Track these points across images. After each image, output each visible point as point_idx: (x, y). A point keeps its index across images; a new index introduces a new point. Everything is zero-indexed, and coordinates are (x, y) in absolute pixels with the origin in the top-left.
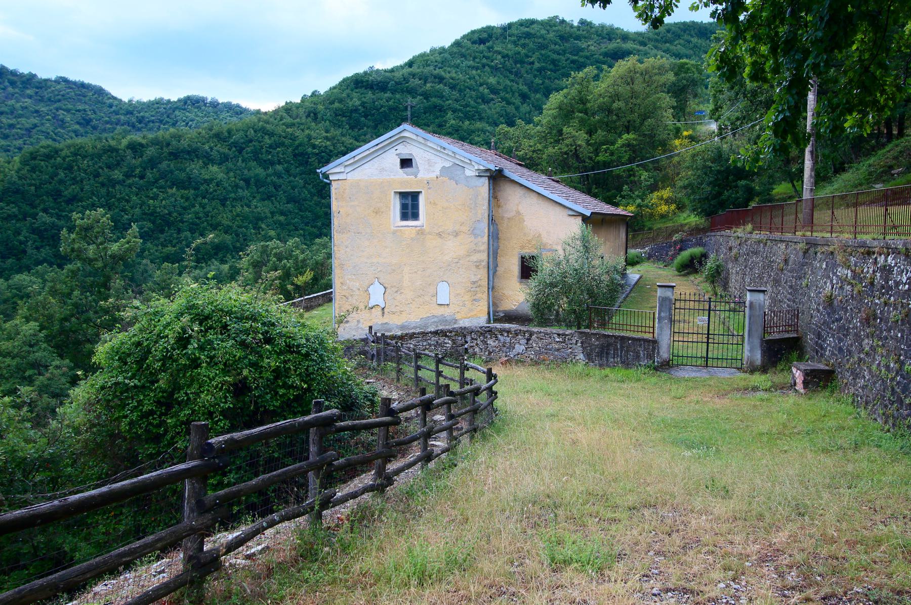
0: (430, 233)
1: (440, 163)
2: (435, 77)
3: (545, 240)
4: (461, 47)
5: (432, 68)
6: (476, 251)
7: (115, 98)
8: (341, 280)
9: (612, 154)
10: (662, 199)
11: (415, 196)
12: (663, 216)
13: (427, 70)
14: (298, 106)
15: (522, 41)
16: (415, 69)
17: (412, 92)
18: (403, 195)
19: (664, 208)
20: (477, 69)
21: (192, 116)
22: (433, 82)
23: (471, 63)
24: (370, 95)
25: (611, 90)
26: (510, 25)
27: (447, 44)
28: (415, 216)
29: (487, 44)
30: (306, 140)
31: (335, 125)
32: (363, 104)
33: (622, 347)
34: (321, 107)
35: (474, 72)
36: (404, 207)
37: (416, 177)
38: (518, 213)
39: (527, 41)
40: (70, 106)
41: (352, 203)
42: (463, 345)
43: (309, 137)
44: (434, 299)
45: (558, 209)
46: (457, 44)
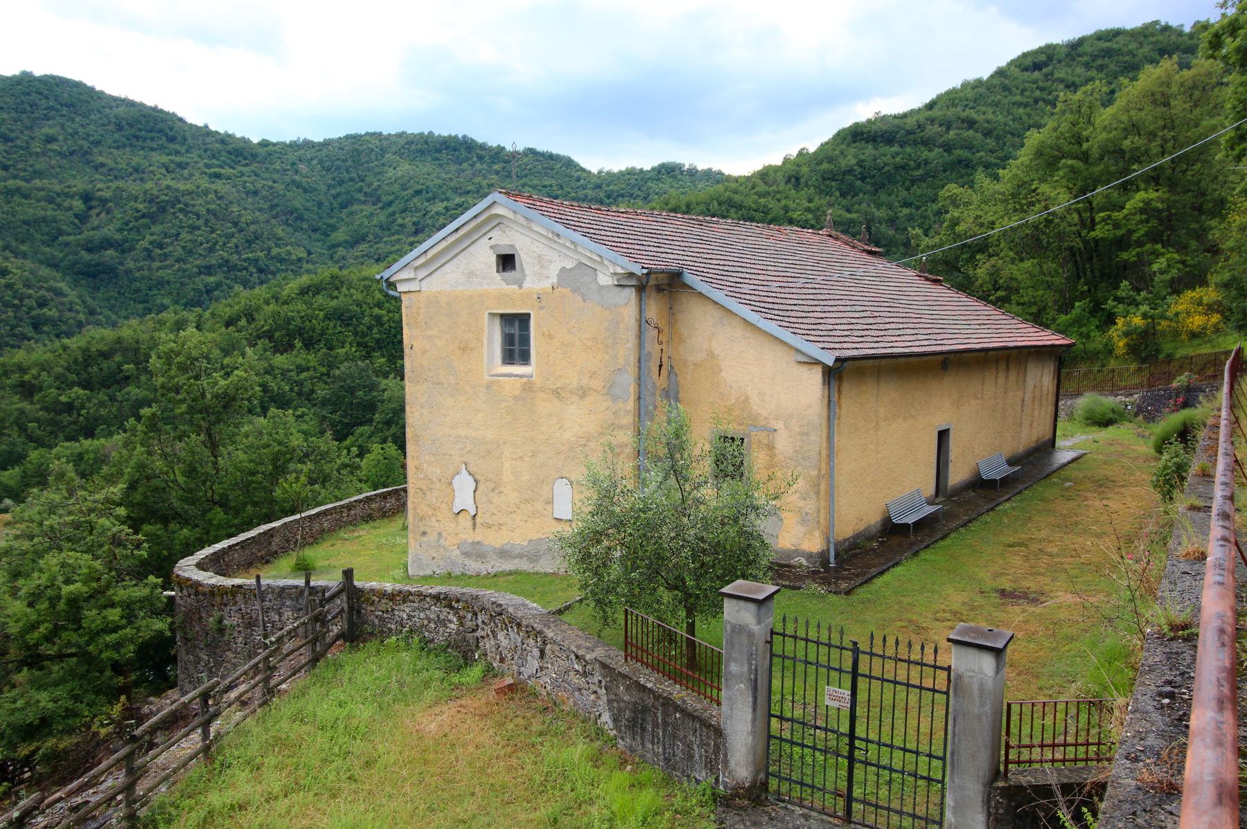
0: (542, 390)
1: (559, 262)
2: (963, 121)
3: (756, 409)
4: (1006, 77)
5: (959, 109)
6: (615, 427)
7: (583, 170)
8: (416, 463)
9: (1116, 226)
10: (1200, 304)
11: (524, 319)
12: (1194, 335)
13: (951, 113)
14: (776, 169)
15: (1099, 62)
16: (936, 113)
17: (927, 143)
18: (507, 319)
19: (1197, 321)
20: (1026, 105)
21: (666, 187)
22: (959, 129)
23: (1018, 98)
24: (869, 151)
25: (1124, 118)
26: (1082, 41)
27: (985, 73)
28: (525, 358)
29: (1045, 70)
30: (782, 212)
31: (821, 192)
32: (860, 163)
33: (665, 724)
34: (805, 169)
35: (1021, 110)
36: (508, 340)
37: (521, 287)
38: (711, 353)
39: (1107, 60)
40: (535, 182)
41: (430, 333)
42: (474, 631)
43: (786, 209)
44: (548, 507)
45: (779, 349)
46: (1000, 73)
